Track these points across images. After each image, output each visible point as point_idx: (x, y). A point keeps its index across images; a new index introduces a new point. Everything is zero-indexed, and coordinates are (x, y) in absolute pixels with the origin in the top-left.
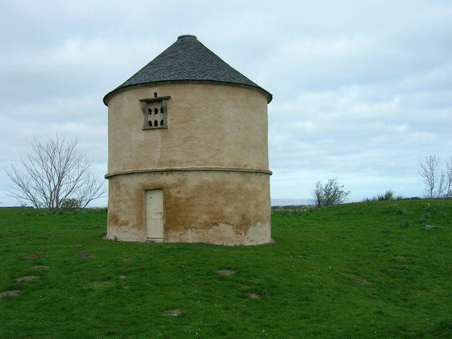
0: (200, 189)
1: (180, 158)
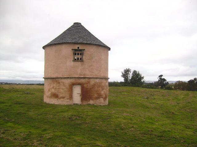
0: (94, 85)
1: (88, 74)
